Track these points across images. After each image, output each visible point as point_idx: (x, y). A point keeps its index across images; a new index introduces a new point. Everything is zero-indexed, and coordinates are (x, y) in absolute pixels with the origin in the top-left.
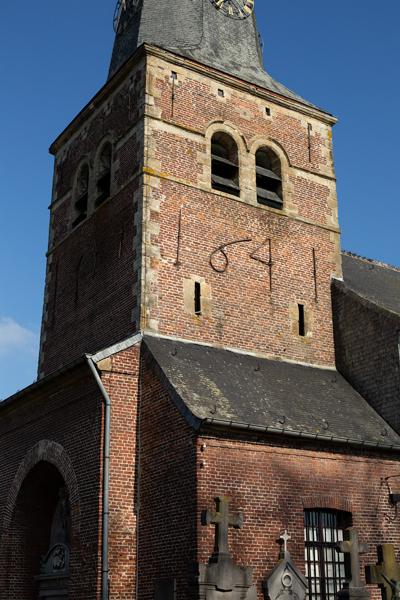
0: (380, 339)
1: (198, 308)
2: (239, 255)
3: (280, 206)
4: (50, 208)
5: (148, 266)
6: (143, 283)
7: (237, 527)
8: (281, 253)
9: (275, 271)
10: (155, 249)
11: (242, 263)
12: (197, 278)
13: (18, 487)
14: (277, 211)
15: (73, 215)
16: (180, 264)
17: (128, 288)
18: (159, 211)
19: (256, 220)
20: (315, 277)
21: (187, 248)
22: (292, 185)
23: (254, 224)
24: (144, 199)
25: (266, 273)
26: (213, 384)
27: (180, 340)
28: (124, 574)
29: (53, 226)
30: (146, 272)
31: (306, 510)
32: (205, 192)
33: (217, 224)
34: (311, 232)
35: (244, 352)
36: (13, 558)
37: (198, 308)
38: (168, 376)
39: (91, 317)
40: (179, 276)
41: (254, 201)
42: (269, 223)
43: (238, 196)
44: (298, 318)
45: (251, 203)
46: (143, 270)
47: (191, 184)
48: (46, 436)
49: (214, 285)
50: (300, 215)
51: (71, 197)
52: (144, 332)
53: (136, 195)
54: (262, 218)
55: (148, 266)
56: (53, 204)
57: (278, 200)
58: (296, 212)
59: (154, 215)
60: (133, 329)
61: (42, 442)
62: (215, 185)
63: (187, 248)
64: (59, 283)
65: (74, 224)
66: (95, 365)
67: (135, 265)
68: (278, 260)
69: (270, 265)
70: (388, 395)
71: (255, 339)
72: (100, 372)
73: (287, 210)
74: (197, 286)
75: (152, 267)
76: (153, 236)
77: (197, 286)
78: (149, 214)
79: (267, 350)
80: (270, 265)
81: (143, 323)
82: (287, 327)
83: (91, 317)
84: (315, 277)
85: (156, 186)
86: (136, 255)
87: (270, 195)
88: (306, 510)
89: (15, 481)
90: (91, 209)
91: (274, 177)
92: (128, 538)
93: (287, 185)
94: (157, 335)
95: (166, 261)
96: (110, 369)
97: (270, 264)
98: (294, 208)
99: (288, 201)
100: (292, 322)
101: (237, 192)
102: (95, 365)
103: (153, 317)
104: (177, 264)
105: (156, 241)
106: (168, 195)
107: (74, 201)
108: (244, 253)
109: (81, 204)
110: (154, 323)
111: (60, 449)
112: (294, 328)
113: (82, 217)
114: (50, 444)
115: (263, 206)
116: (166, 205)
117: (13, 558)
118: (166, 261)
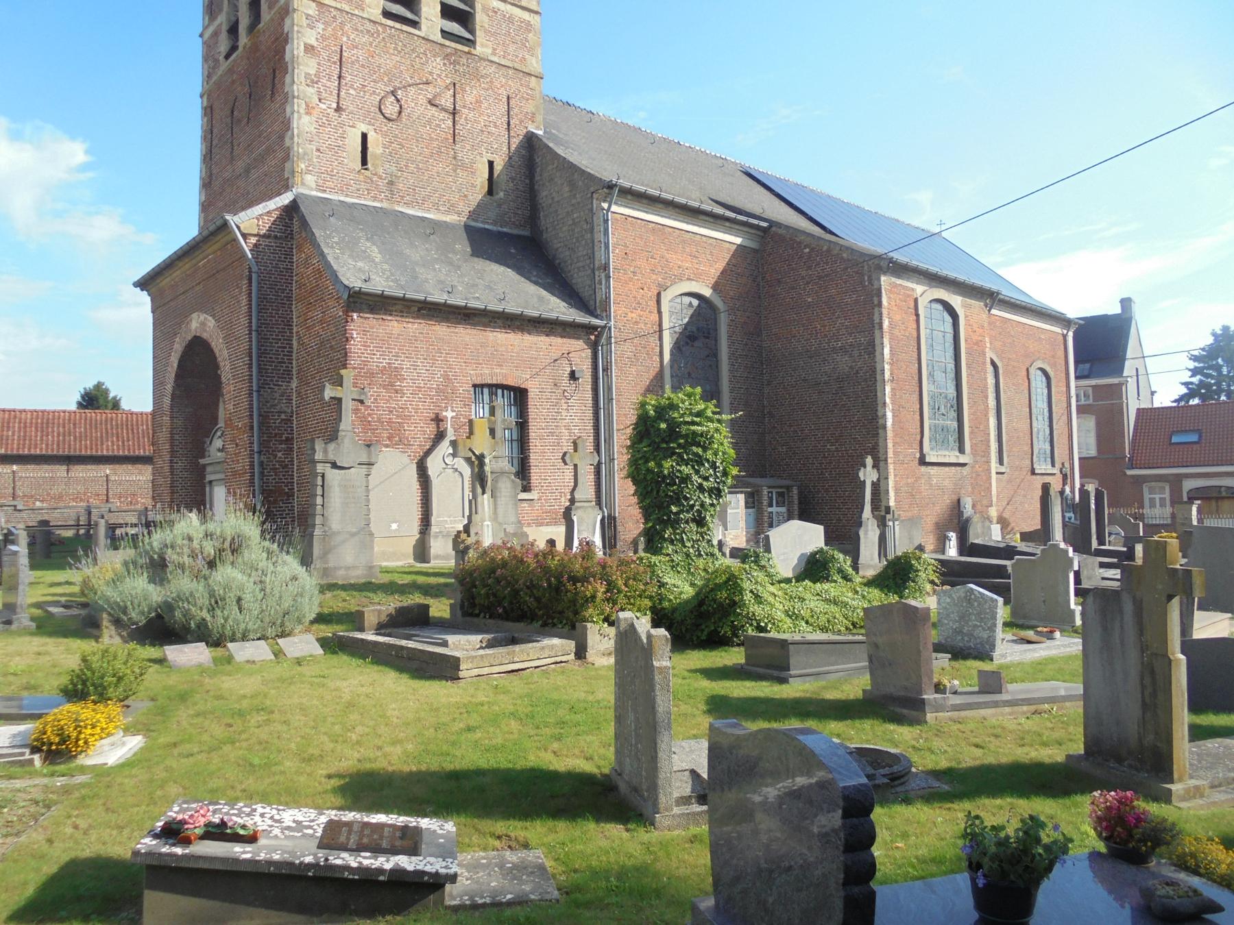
0: (574, 201)
1: (364, 162)
2: (415, 101)
3: (471, 43)
4: (201, 36)
5: (302, 111)
6: (296, 131)
7: (362, 402)
8: (470, 99)
9: (461, 120)
10: (311, 91)
11: (420, 110)
12: (363, 128)
13: (175, 365)
14: (466, 49)
15: (223, 45)
16: (344, 110)
17: (282, 138)
18: (315, 44)
19: (438, 60)
20: (508, 129)
21: (352, 91)
22: (486, 19)
23: (436, 65)
24: (296, 28)
25: (450, 123)
26: (374, 248)
27: (342, 198)
28: (280, 454)
29: (206, 59)
30: (300, 118)
31: (475, 386)
32: (374, 22)
33: (388, 61)
34: (505, 76)
35: (420, 214)
36: (177, 443)
37: (364, 162)
38: (320, 240)
39: (247, 171)
40: (342, 125)
41: (438, 37)
42: (455, 63)
43: (420, 29)
44: (486, 176)
45: (432, 37)
46: (296, 115)
47: (356, 12)
48: (202, 308)
49: (385, 135)
50: (494, 54)
51: (221, 24)
52: (298, 190)
53: (288, 22)
54: (447, 56)
55: (302, 111)
56: (205, 28)
57: (467, 35)
58: (490, 51)
59: (309, 49)
60: (287, 188)
61: (195, 315)
62: (387, 14)
63: (352, 91)
64: (215, 131)
65: (227, 57)
66: (238, 227)
67: (288, 109)
68: (464, 107)
69: (454, 114)
70: (580, 264)
71: (435, 198)
72: (245, 236)
73: (479, 50)
74: (364, 137)
75: (307, 113)
76: (307, 75)
77: (364, 137)
78: (302, 47)
79: (448, 212)
80: (454, 114)
81: (298, 179)
82: (473, 186)
83: (247, 171)
84: (508, 129)
85: (311, 12)
86: (287, 98)
87: (455, 27)
88: (475, 386)
89: (172, 359)
90: (243, 40)
91: (467, 8)
92: (283, 416)
93: (480, 18)
94: (314, 193)
95: (324, 106)
96: (255, 232)
97: (454, 113)
98: (486, 46)
99: (480, 36)
100: (480, 180)
101: (414, 24)
102: (238, 227)
103: (309, 172)
104: (338, 109)
105: (312, 82)
106: (325, 23)
107: (225, 28)
108: (422, 100)
109: (233, 30)
110: (310, 179)
111: (211, 322)
112: (482, 187)
113: (234, 48)
114: (202, 318)
115: (447, 43)
116: (324, 38)
117: (177, 443)
118: (324, 106)
